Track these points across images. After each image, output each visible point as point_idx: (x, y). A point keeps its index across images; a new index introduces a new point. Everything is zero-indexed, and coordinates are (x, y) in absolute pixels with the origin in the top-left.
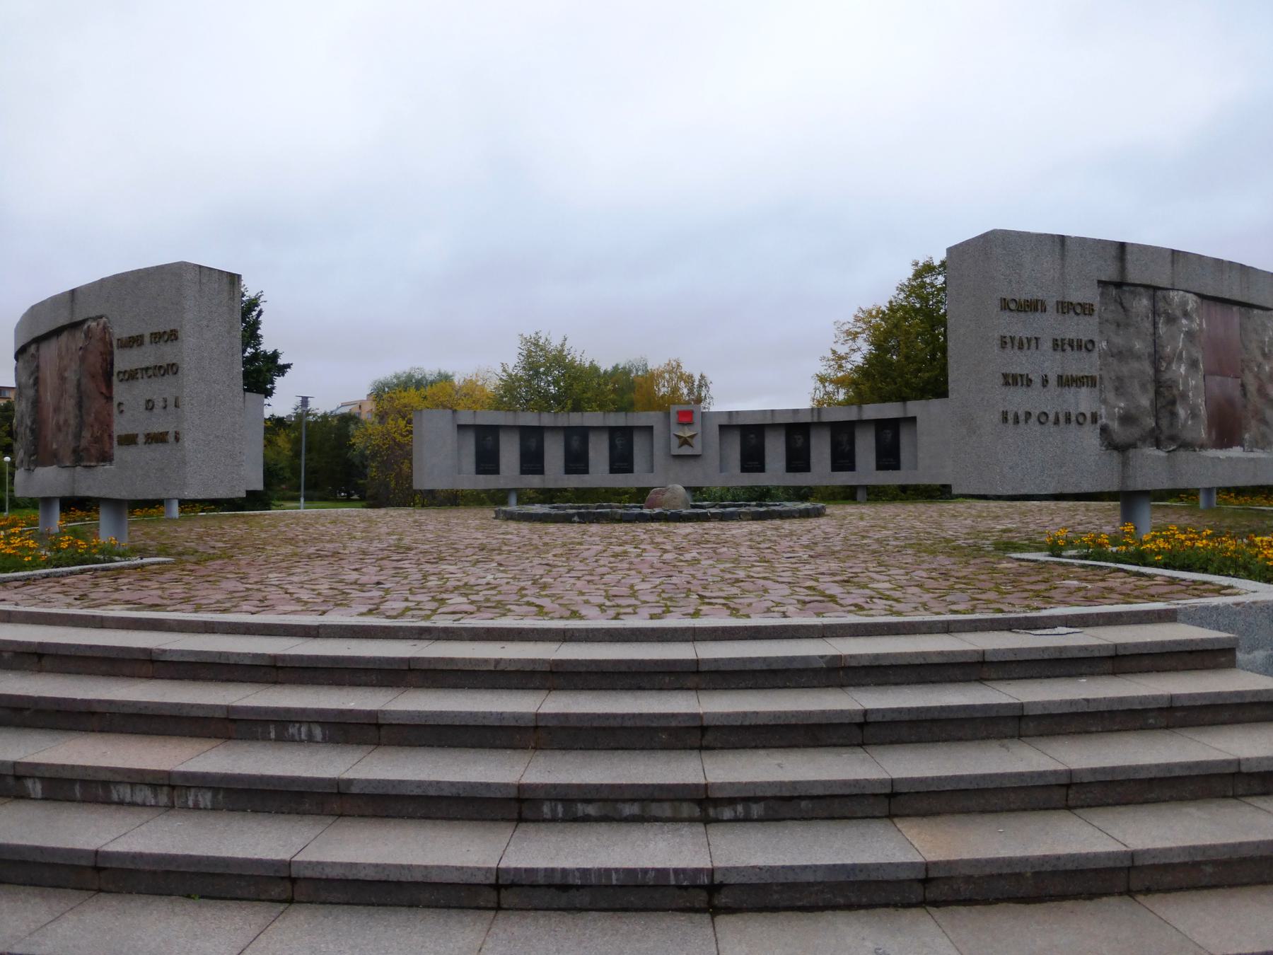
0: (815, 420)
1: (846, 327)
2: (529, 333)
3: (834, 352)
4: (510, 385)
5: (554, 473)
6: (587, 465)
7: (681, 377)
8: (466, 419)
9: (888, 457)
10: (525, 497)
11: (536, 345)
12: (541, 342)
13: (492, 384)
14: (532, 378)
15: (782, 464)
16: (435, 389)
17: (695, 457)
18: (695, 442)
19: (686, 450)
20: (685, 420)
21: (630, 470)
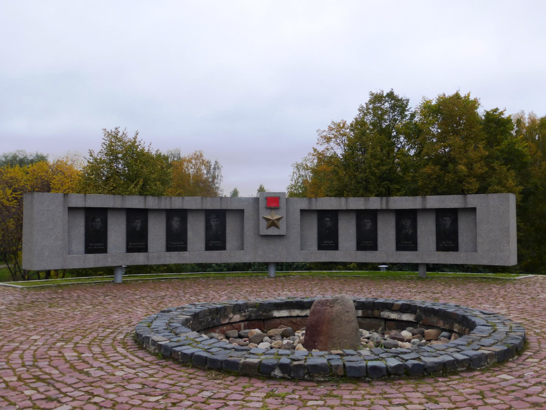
0: (384, 207)
1: (324, 134)
2: (111, 128)
3: (315, 150)
4: (95, 167)
5: (157, 250)
6: (186, 243)
7: (203, 163)
8: (77, 201)
9: (447, 240)
10: (132, 270)
11: (116, 137)
12: (120, 134)
13: (81, 164)
14: (111, 162)
15: (353, 243)
16: (35, 167)
17: (280, 236)
18: (282, 224)
19: (273, 231)
20: (273, 205)
21: (223, 248)
